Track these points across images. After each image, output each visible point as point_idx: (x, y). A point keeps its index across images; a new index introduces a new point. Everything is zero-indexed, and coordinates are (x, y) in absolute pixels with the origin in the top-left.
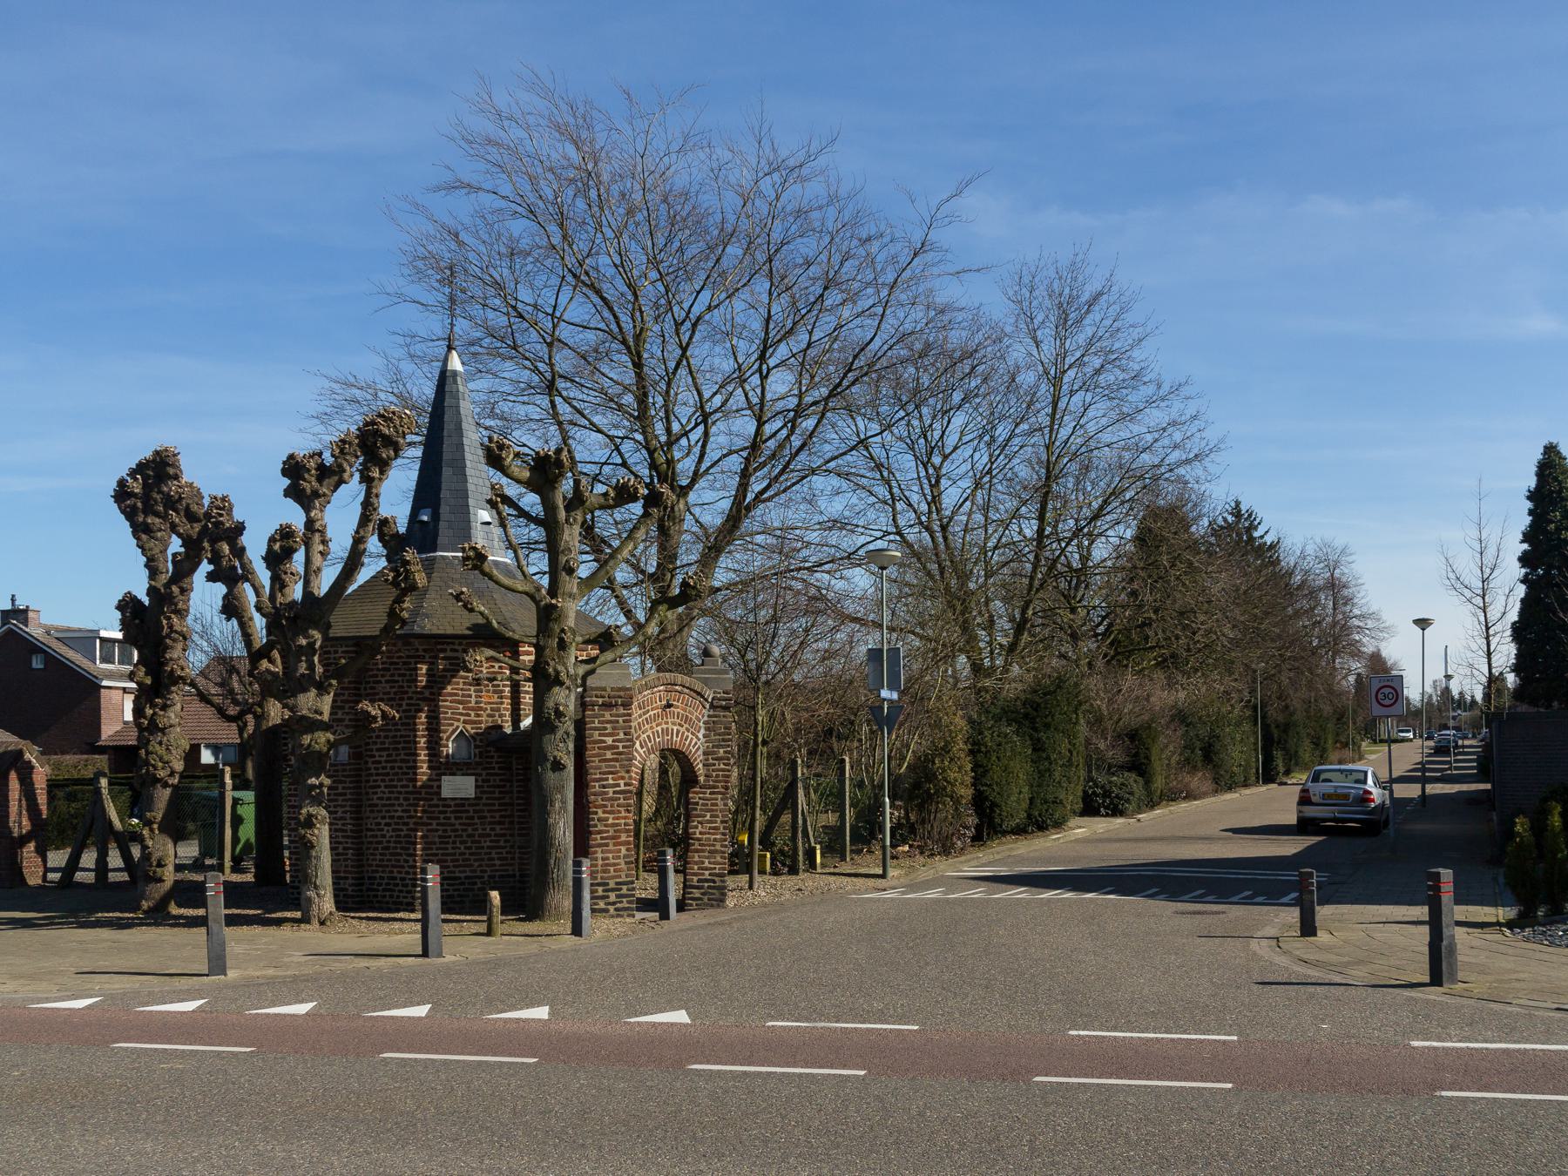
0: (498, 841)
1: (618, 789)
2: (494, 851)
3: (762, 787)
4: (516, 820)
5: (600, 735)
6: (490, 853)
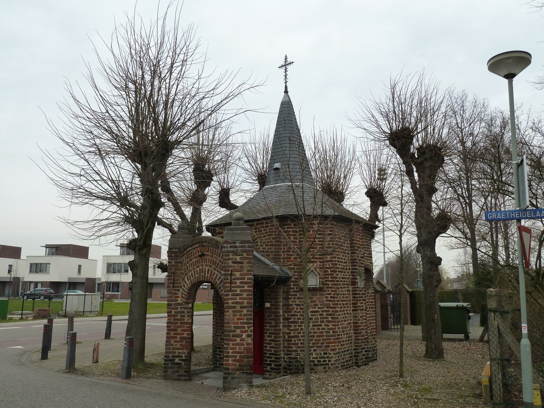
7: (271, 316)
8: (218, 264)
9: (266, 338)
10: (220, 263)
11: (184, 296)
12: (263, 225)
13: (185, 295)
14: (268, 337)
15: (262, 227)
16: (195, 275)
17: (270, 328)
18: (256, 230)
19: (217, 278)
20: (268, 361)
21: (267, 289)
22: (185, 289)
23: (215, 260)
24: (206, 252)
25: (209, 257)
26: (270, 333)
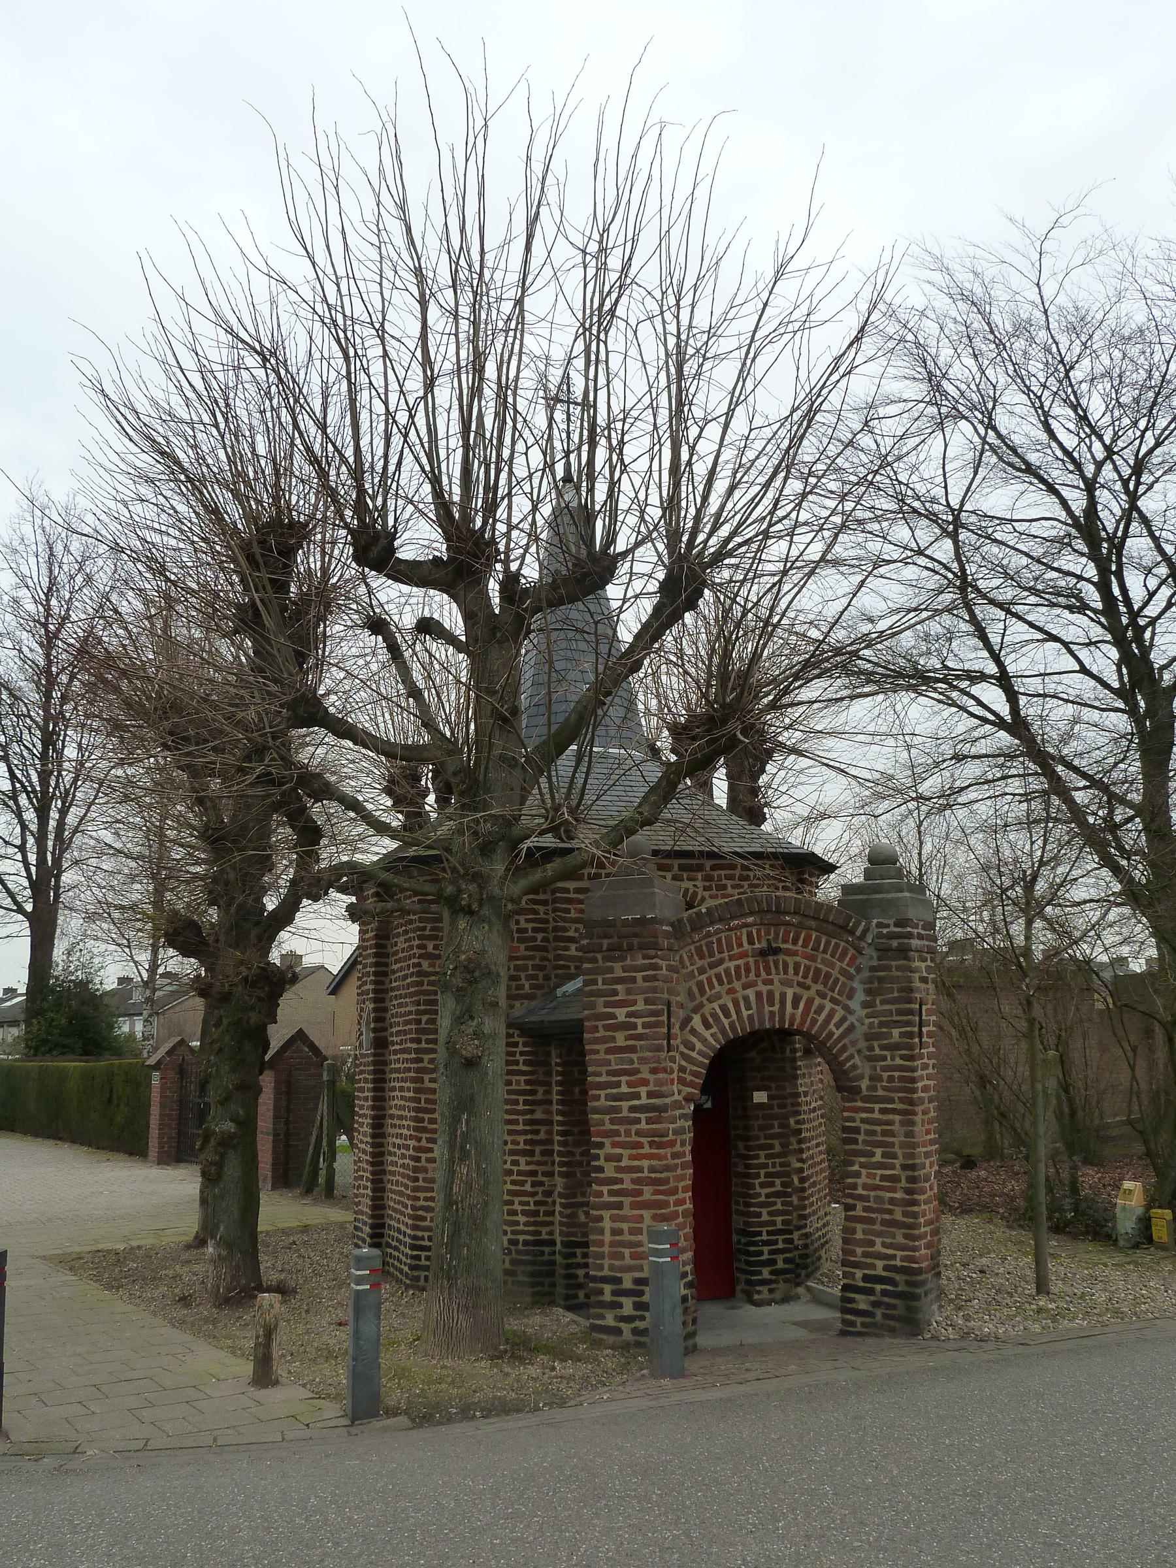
0: (522, 1183)
1: (636, 1102)
2: (517, 1200)
3: (248, 1125)
4: (556, 1148)
5: (607, 1005)
6: (511, 1203)
7: (772, 1127)
8: (837, 980)
9: (758, 1190)
10: (842, 979)
11: (689, 1078)
12: (731, 872)
13: (693, 1073)
14: (762, 1185)
15: (728, 877)
16: (738, 1012)
17: (770, 1162)
18: (707, 884)
19: (834, 1021)
20: (766, 1252)
21: (753, 1054)
22: (694, 1054)
23: (825, 969)
24: (785, 941)
25: (798, 959)
26: (767, 1175)
